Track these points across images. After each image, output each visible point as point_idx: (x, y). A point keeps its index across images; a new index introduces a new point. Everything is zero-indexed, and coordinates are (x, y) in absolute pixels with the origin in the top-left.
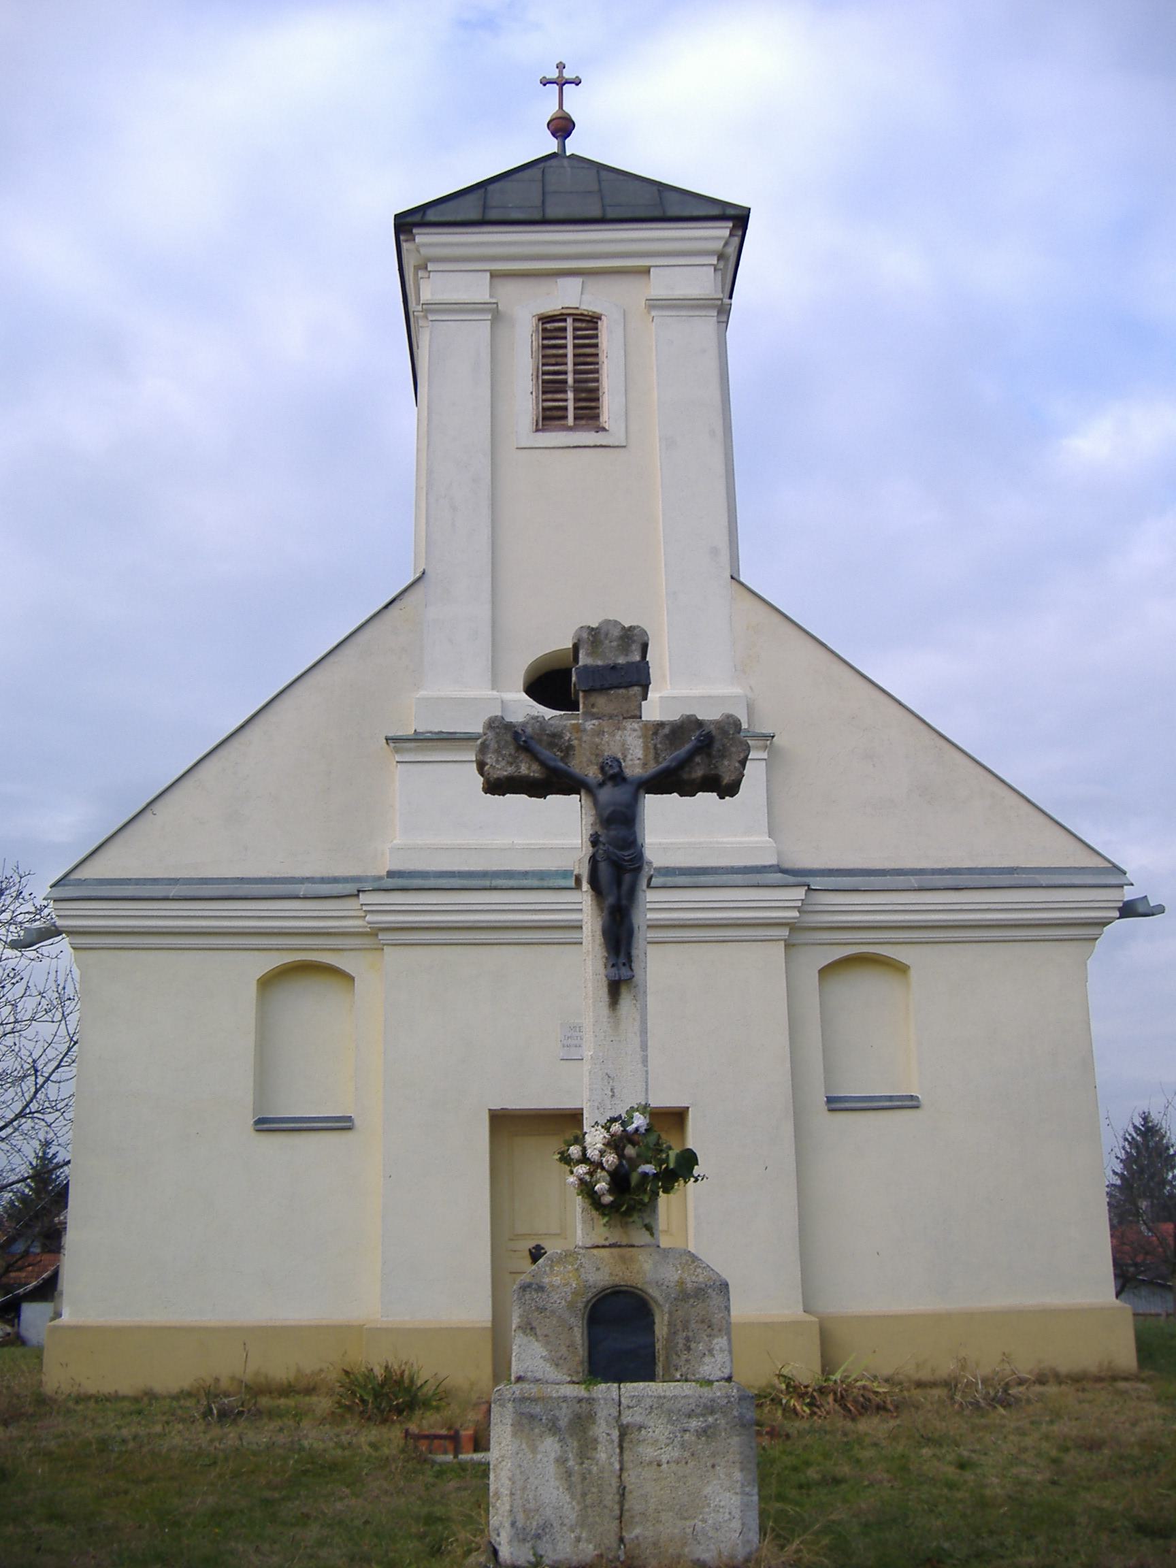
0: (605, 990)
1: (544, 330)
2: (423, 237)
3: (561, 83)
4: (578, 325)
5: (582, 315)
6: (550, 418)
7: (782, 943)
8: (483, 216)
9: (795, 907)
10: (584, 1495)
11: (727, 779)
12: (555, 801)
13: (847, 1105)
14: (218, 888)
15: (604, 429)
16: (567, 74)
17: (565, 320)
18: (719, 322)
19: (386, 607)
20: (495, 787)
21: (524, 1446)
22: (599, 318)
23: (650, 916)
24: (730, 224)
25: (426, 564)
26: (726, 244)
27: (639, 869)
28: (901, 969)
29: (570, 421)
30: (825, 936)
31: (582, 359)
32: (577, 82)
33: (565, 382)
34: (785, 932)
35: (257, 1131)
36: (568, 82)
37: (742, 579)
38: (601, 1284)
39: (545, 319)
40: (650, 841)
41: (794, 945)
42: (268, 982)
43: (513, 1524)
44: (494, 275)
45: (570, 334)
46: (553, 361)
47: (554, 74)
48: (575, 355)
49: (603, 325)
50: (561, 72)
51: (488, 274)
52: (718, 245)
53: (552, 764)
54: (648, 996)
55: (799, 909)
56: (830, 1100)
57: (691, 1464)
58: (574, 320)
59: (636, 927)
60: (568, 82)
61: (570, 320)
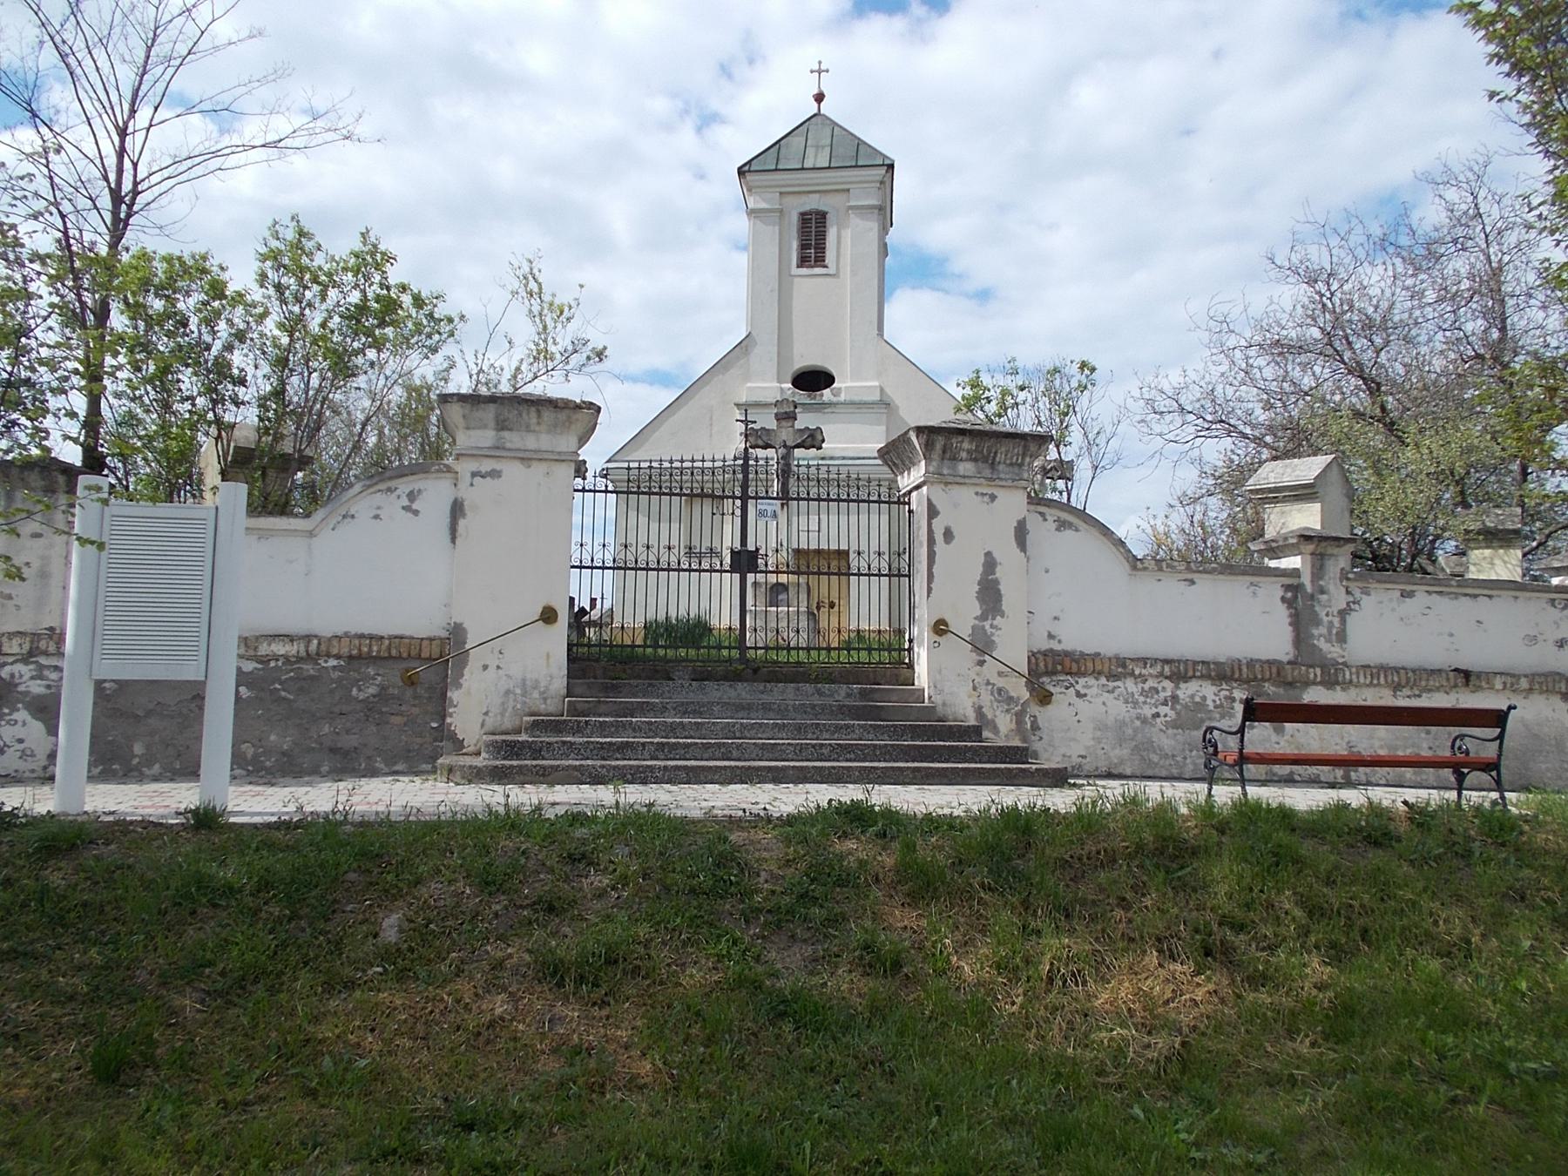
2: (749, 177)
3: (820, 72)
6: (803, 261)
32: (827, 71)
39: (803, 214)
44: (781, 193)
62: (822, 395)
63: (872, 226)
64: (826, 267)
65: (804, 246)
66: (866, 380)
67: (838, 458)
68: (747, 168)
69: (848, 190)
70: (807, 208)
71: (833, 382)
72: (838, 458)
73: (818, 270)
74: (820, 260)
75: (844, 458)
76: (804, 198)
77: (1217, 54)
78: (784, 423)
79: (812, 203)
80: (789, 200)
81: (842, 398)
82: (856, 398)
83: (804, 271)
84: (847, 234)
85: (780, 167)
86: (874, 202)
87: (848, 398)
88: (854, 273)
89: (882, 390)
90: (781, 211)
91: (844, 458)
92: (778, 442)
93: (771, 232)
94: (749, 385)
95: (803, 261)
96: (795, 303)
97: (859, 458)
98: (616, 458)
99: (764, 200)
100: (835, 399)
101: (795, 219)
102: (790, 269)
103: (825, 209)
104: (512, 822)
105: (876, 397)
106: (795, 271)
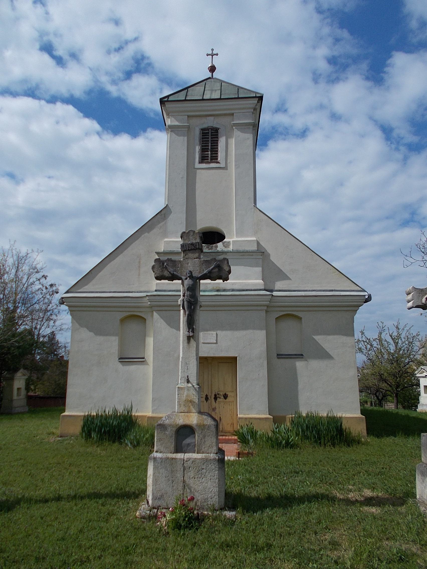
0: (186, 338)
1: (203, 133)
2: (168, 105)
3: (212, 55)
4: (213, 131)
5: (214, 128)
6: (203, 159)
8: (210, 97)
9: (268, 301)
10: (173, 486)
11: (224, 276)
13: (283, 357)
15: (219, 163)
16: (215, 52)
17: (209, 130)
18: (253, 130)
19: (156, 215)
21: (156, 472)
22: (219, 129)
24: (257, 99)
25: (168, 203)
26: (256, 105)
28: (300, 318)
29: (209, 160)
31: (204, 140)
32: (217, 55)
33: (208, 149)
34: (266, 308)
35: (120, 362)
36: (214, 55)
39: (203, 130)
41: (268, 311)
42: (123, 321)
43: (153, 494)
44: (188, 116)
45: (210, 134)
46: (205, 142)
47: (210, 52)
48: (211, 141)
49: (219, 131)
50: (212, 52)
51: (187, 117)
52: (253, 106)
56: (278, 355)
57: (204, 479)
58: (211, 130)
59: (195, 320)
60: (214, 55)
61: (210, 130)
62: (217, 247)
63: (249, 137)
64: (219, 163)
65: (203, 150)
66: (247, 236)
67: (229, 290)
68: (166, 99)
69: (233, 114)
70: (205, 126)
71: (225, 238)
72: (229, 290)
73: (213, 165)
74: (214, 159)
75: (233, 290)
76: (204, 120)
77: (350, 162)
78: (190, 255)
79: (209, 123)
80: (194, 122)
81: (231, 248)
82: (241, 249)
83: (204, 165)
84: (232, 142)
85: (187, 98)
86: (251, 121)
87: (235, 249)
88: (237, 166)
89: (258, 243)
90: (189, 127)
91: (233, 290)
92: (184, 273)
93: (182, 141)
94: (166, 240)
95: (203, 159)
96: (198, 185)
97: (243, 290)
98: (72, 290)
99: (177, 121)
100: (225, 250)
101: (197, 132)
102: (194, 164)
103: (218, 126)
104: (246, 279)
105: (255, 248)
106: (197, 165)
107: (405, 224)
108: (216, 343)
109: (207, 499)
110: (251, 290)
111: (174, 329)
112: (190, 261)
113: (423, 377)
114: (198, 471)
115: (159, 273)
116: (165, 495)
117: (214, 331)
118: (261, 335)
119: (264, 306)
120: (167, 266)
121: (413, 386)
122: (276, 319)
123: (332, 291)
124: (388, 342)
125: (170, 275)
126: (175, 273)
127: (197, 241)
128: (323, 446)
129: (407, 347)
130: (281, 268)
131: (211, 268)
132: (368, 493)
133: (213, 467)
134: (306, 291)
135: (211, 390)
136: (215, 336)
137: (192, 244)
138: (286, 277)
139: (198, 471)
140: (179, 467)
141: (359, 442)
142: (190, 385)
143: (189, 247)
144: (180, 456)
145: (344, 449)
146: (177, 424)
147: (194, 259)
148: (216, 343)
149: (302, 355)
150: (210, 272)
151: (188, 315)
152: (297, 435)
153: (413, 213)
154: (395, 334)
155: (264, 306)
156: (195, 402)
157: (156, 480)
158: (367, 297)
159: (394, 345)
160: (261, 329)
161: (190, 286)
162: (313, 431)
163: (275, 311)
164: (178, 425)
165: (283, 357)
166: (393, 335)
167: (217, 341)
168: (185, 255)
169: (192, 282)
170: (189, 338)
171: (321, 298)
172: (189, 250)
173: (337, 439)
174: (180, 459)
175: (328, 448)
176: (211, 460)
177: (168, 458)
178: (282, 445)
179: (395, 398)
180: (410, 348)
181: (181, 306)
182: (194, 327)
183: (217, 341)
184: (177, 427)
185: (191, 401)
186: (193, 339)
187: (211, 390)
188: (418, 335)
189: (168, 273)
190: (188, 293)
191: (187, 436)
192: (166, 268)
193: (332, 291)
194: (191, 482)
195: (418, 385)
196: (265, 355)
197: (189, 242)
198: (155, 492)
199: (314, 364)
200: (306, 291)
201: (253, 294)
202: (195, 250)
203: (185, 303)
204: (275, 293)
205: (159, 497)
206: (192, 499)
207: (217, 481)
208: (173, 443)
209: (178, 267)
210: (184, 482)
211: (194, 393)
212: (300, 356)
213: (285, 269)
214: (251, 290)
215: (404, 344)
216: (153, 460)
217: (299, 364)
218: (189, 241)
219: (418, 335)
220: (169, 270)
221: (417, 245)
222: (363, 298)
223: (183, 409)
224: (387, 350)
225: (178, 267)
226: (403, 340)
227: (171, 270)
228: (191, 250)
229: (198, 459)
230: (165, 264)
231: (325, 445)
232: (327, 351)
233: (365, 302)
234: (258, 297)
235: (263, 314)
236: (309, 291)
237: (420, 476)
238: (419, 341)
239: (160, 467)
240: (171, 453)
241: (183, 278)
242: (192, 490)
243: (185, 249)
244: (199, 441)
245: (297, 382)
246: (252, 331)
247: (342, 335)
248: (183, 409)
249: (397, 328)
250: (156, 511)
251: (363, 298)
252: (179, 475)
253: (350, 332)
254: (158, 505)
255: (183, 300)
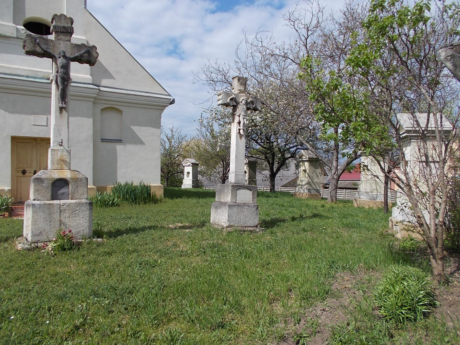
0: (59, 109)
7: (92, 102)
10: (50, 225)
11: (93, 61)
12: (45, 59)
14: (43, 69)
20: (29, 53)
23: (71, 93)
27: (69, 80)
28: (121, 112)
30: (104, 102)
34: (93, 100)
37: (87, 9)
38: (56, 178)
40: (73, 74)
43: (32, 232)
53: (45, 49)
54: (4, 112)
55: (97, 94)
56: (102, 139)
107: (170, 53)
108: (47, 126)
109: (80, 231)
110: (81, 83)
111: (2, 110)
112: (62, 42)
113: (187, 166)
114: (72, 212)
115: (29, 47)
116: (43, 232)
117: (44, 115)
118: (88, 122)
119: (92, 98)
120: (40, 43)
121: (178, 173)
122: (102, 110)
123: (147, 92)
124: (165, 141)
125: (42, 52)
126: (48, 50)
127: (68, 26)
128: (138, 204)
129: (177, 145)
130: (107, 68)
131: (82, 52)
132: (180, 224)
133: (85, 208)
134: (127, 90)
135: (40, 166)
136: (46, 119)
137: (64, 27)
138: (110, 77)
139: (72, 212)
140: (56, 210)
141: (161, 201)
142: (62, 148)
143: (61, 30)
144: (55, 202)
145: (153, 205)
146: (53, 178)
147: (66, 41)
148: (47, 126)
149: (121, 140)
150: (81, 56)
151: (62, 89)
152: (118, 198)
153: (176, 47)
154: (170, 135)
155: (92, 98)
156: (67, 162)
157: (35, 221)
158: (172, 100)
159: (168, 143)
160: (89, 117)
161: (64, 64)
162: (131, 195)
163: (100, 103)
164: (54, 178)
165: (104, 141)
166: (168, 136)
167: (47, 124)
168: (58, 36)
169: (66, 61)
170: (61, 109)
171: (140, 97)
172: (61, 32)
173: (148, 199)
174: (57, 204)
175: (141, 206)
176: (83, 203)
177: (46, 204)
178: (109, 205)
179: (166, 182)
180: (180, 146)
181: (54, 82)
182: (66, 100)
183: (47, 124)
184: (53, 181)
185: (63, 161)
186: (65, 110)
187: (40, 166)
188: (185, 137)
189: (41, 49)
190: (62, 70)
191: (62, 187)
192: (38, 44)
193: (147, 92)
194: (66, 221)
195: (182, 172)
196: (91, 138)
197: (61, 25)
198: (34, 230)
199: (130, 148)
200: (127, 90)
201: (83, 86)
202: (67, 33)
203: (59, 78)
204: (102, 89)
205: (38, 234)
206: (70, 231)
207: (88, 218)
208: (50, 193)
209: (50, 46)
210: (60, 221)
211: (66, 154)
212: (119, 141)
213: (111, 69)
214: (81, 83)
215: (176, 143)
216: (32, 206)
217: (119, 147)
218: (61, 24)
219: (185, 137)
220: (42, 47)
221: (202, 69)
222: (169, 101)
223: (56, 166)
224: (164, 147)
225: (50, 46)
226: (175, 140)
227: (44, 47)
228: (63, 32)
229: (73, 203)
230: (38, 41)
231: (139, 204)
232: (140, 139)
233: (170, 104)
234: (86, 90)
235: (91, 104)
236: (130, 90)
237: (214, 209)
238: (186, 141)
239: (38, 211)
240: (48, 200)
241: (57, 56)
242: (67, 227)
243: (57, 30)
244: (73, 190)
245: (116, 161)
246: (80, 118)
247: (152, 127)
248: (56, 166)
249: (172, 131)
250: (36, 244)
251: (169, 101)
252: (56, 216)
253: (157, 124)
254: (37, 240)
255: (57, 76)
